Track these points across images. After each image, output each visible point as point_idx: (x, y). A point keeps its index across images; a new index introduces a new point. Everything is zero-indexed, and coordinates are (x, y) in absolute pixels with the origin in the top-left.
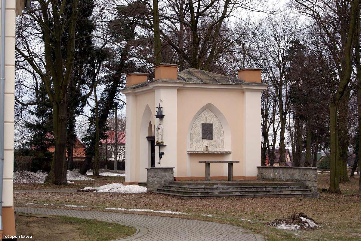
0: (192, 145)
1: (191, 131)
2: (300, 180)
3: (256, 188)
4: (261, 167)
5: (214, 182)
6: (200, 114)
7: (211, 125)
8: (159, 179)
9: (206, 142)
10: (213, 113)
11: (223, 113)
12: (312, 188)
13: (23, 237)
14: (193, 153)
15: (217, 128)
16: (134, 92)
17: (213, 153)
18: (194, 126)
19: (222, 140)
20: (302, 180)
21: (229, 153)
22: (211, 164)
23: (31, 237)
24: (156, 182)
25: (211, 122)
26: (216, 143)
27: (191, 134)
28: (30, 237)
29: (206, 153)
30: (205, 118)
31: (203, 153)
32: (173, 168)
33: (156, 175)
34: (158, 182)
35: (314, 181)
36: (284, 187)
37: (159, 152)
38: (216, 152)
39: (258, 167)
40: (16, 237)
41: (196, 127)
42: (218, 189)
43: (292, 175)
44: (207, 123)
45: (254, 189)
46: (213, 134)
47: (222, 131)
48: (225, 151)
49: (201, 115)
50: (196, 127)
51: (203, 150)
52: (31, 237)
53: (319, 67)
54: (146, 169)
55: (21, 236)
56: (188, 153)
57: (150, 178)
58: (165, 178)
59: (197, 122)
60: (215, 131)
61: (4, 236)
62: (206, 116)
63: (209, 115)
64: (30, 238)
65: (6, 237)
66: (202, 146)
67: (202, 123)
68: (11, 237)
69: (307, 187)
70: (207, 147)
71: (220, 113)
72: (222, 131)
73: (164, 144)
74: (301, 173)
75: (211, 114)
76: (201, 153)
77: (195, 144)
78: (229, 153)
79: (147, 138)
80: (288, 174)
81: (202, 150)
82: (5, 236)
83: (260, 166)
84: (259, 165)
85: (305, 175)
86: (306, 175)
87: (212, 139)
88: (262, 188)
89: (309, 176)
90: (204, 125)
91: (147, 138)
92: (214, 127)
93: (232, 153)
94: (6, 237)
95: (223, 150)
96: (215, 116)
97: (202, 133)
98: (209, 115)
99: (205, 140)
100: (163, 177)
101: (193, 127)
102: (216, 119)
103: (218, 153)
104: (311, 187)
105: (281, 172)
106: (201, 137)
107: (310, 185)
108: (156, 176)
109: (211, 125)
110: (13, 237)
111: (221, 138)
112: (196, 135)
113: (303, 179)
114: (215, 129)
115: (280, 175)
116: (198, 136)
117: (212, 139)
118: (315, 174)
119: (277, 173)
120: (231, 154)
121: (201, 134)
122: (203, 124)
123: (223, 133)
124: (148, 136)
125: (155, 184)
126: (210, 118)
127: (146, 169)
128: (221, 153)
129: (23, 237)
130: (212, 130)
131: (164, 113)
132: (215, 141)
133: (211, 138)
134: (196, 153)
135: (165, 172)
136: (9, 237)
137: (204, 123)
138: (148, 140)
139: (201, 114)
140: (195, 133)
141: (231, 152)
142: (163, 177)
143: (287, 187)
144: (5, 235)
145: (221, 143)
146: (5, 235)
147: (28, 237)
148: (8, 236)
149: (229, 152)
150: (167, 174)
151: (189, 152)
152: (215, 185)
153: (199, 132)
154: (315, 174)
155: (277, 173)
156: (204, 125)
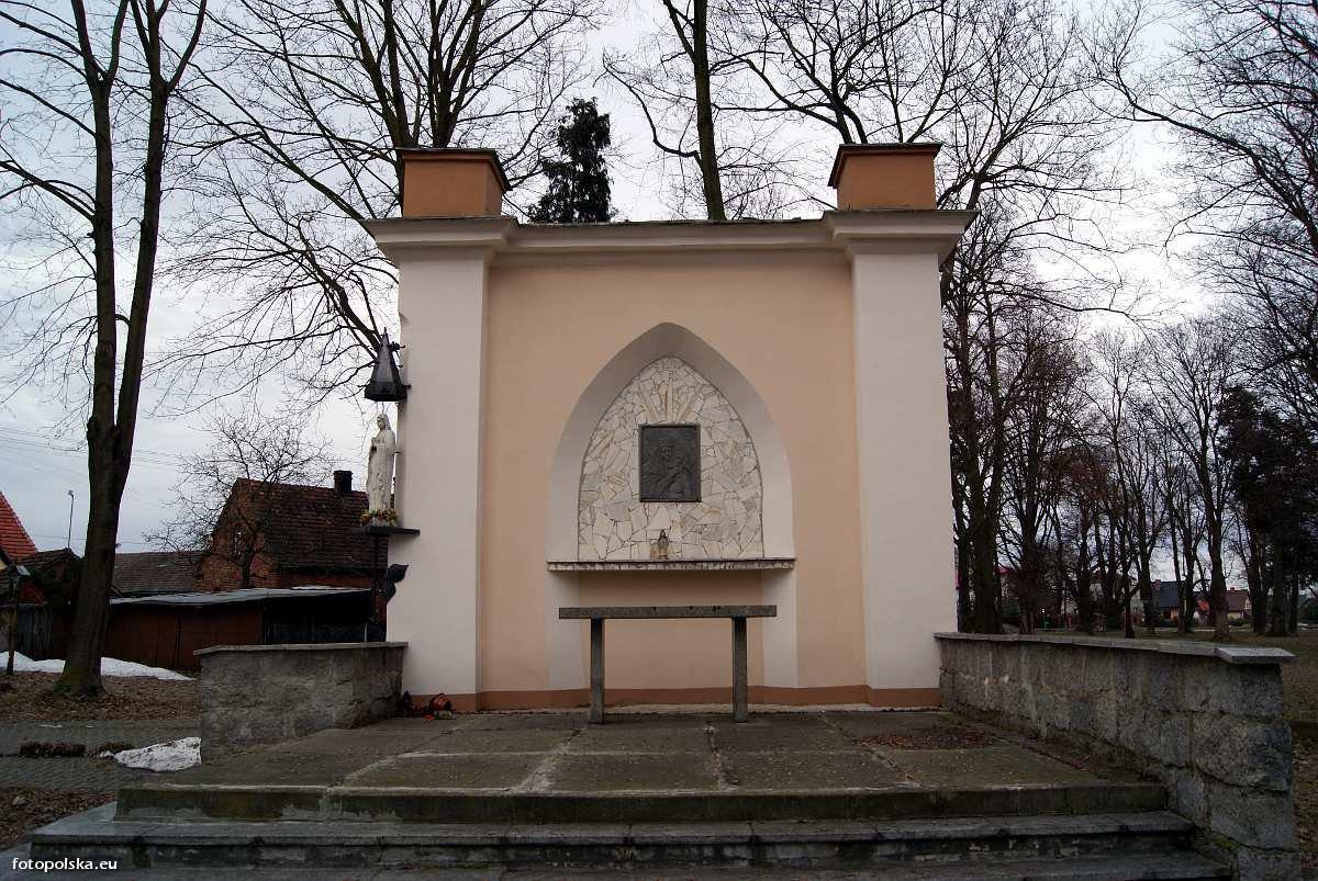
0: (586, 533)
1: (584, 464)
2: (1132, 754)
3: (650, 855)
4: (964, 636)
6: (630, 383)
7: (692, 431)
8: (262, 710)
9: (664, 515)
10: (697, 375)
11: (743, 371)
12: (1243, 854)
13: (84, 865)
14: (581, 568)
15: (722, 444)
17: (691, 567)
18: (598, 439)
19: (749, 505)
20: (1151, 759)
21: (778, 565)
22: (748, 619)
23: (112, 865)
24: (244, 731)
25: (691, 420)
26: (717, 520)
27: (583, 477)
28: (110, 867)
30: (656, 401)
31: (633, 568)
32: (745, 619)
33: (247, 690)
34: (255, 727)
35: (1257, 788)
36: (948, 840)
38: (705, 565)
39: (941, 639)
40: (59, 865)
41: (608, 445)
42: (266, 855)
43: (1082, 700)
44: (668, 422)
45: (632, 859)
46: (704, 476)
47: (749, 463)
48: (769, 556)
49: (634, 388)
50: (608, 445)
51: (646, 556)
52: (112, 865)
53: (1286, 434)
55: (75, 864)
56: (553, 568)
57: (215, 703)
58: (302, 707)
59: (616, 420)
60: (709, 461)
61: (15, 862)
62: (663, 391)
63: (676, 385)
64: (108, 869)
65: (23, 865)
66: (639, 536)
67: (642, 422)
68: (40, 865)
69: (1193, 830)
70: (663, 536)
71: (728, 369)
72: (749, 463)
73: (408, 526)
74: (1137, 693)
75: (686, 378)
76: (623, 568)
77: (603, 524)
78: (778, 565)
80: (1059, 689)
81: (642, 552)
82: (17, 864)
83: (954, 628)
84: (951, 627)
85: (1166, 712)
86: (1177, 719)
87: (699, 500)
88: (718, 846)
89: (1203, 728)
90: (651, 436)
92: (705, 440)
93: (796, 563)
94: (23, 865)
95: (754, 554)
96: (711, 390)
97: (642, 473)
98: (676, 385)
99: (657, 504)
100: (287, 703)
101: (595, 442)
102: (714, 401)
103: (717, 567)
104: (1230, 846)
105: (1025, 670)
106: (636, 490)
107: (1222, 825)
108: (244, 697)
109: (692, 431)
110: (49, 865)
111: (745, 495)
112: (609, 480)
113: (1160, 746)
114: (710, 452)
115: (1022, 693)
116: (618, 489)
117: (699, 500)
118: (1268, 720)
119: (1006, 679)
120: (794, 573)
121: (635, 476)
122: (644, 428)
123: (757, 467)
125: (241, 741)
126: (682, 399)
128: (738, 567)
129: (84, 865)
130: (698, 458)
131: (411, 377)
132: (712, 511)
133: (690, 492)
134: (598, 567)
135: (299, 674)
136: (33, 865)
137: (650, 423)
139: (636, 383)
140: (606, 473)
141: (791, 561)
142: (287, 703)
143: (980, 840)
145: (748, 518)
148: (30, 862)
149: (782, 561)
150: (310, 685)
151: (556, 563)
152: (289, 811)
153: (627, 468)
154: (1268, 720)
155: (1006, 679)
156: (651, 436)
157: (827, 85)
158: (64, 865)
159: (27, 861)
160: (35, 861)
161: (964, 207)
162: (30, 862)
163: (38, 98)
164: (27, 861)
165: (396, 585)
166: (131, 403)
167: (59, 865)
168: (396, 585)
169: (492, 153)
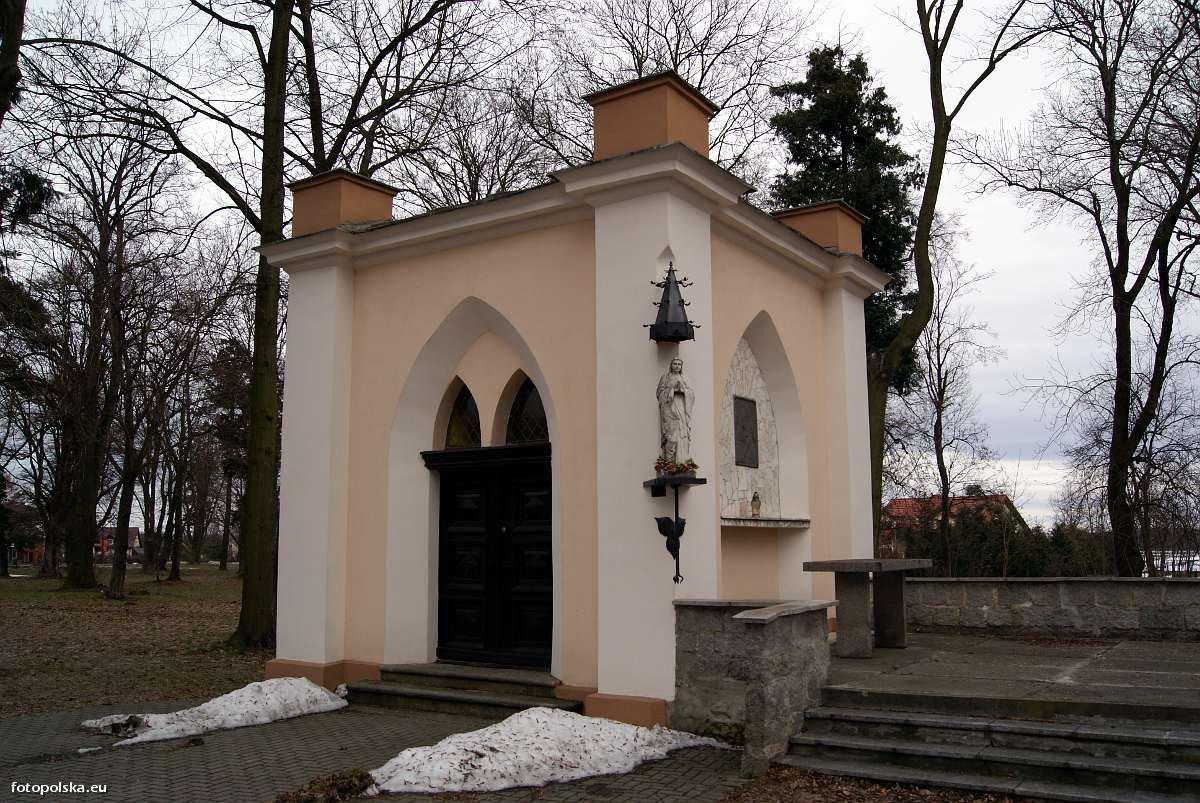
5: (1099, 751)
13: (76, 788)
16: (360, 249)
23: (102, 789)
28: (101, 791)
29: (749, 524)
37: (878, 509)
40: (54, 789)
52: (102, 789)
54: (703, 481)
55: (68, 788)
61: (13, 786)
64: (99, 793)
65: (21, 788)
68: (36, 789)
78: (797, 526)
79: (426, 456)
82: (16, 788)
91: (426, 456)
94: (21, 788)
110: (45, 788)
120: (810, 530)
124: (430, 448)
127: (703, 481)
129: (76, 788)
136: (30, 788)
138: (429, 468)
141: (808, 522)
144: (17, 785)
146: (17, 785)
147: (92, 788)
157: (1091, 206)
158: (58, 789)
159: (25, 785)
160: (32, 785)
161: (484, 196)
162: (28, 785)
163: (811, 242)
164: (25, 785)
165: (805, 81)
166: (941, 109)
167: (54, 789)
168: (805, 81)
169: (253, 27)
